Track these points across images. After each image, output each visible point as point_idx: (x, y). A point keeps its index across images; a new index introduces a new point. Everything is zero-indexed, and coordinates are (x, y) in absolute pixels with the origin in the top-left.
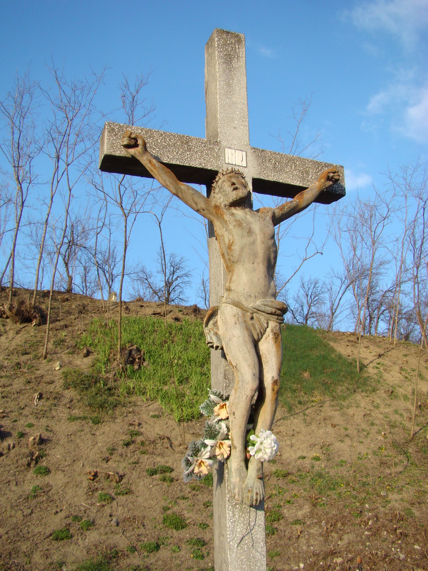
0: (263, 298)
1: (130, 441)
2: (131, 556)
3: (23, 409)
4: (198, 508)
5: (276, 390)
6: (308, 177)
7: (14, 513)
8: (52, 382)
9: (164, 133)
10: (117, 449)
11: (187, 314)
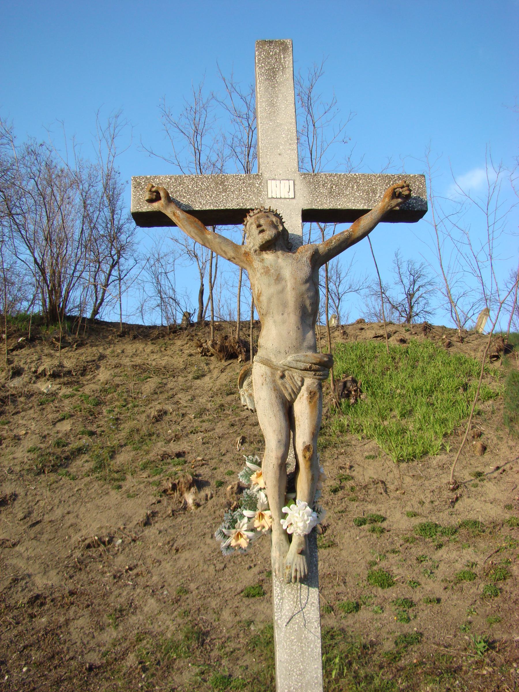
0: (295, 353)
1: (338, 486)
2: (326, 616)
3: (224, 455)
4: (410, 563)
5: (308, 457)
6: (375, 197)
7: (207, 567)
9: (196, 177)
10: (322, 497)
11: (416, 333)
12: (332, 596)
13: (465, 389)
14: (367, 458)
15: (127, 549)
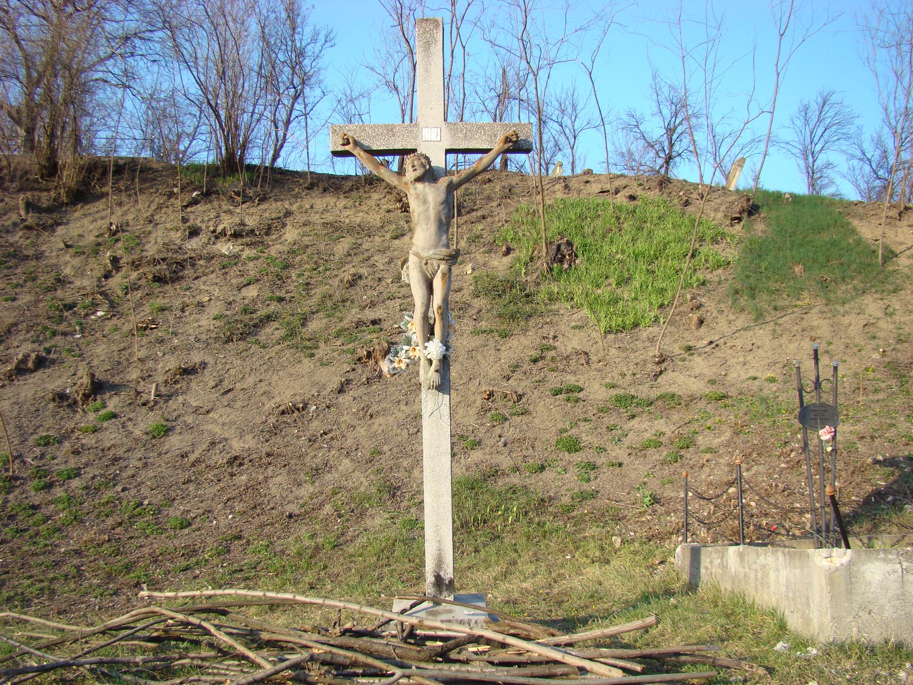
8: (460, 290)
11: (649, 188)
14: (574, 328)
15: (322, 415)
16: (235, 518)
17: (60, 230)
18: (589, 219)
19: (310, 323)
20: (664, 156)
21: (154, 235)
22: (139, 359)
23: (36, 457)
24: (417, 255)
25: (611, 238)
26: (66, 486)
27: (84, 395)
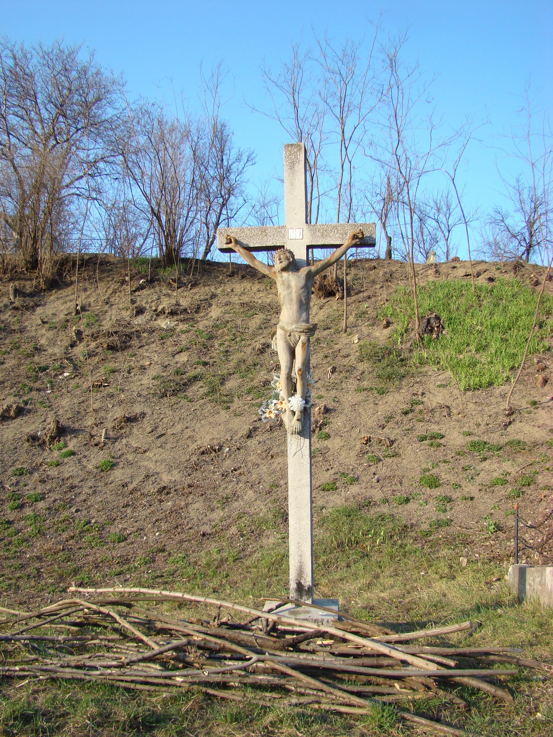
4: (457, 471)
8: (348, 356)
11: (506, 272)
12: (390, 492)
13: (541, 327)
14: (439, 386)
16: (161, 535)
17: (39, 310)
18: (454, 298)
19: (227, 383)
20: (525, 245)
21: (109, 313)
22: (94, 410)
23: (13, 484)
24: (283, 328)
25: (472, 313)
26: (34, 507)
27: (51, 437)
